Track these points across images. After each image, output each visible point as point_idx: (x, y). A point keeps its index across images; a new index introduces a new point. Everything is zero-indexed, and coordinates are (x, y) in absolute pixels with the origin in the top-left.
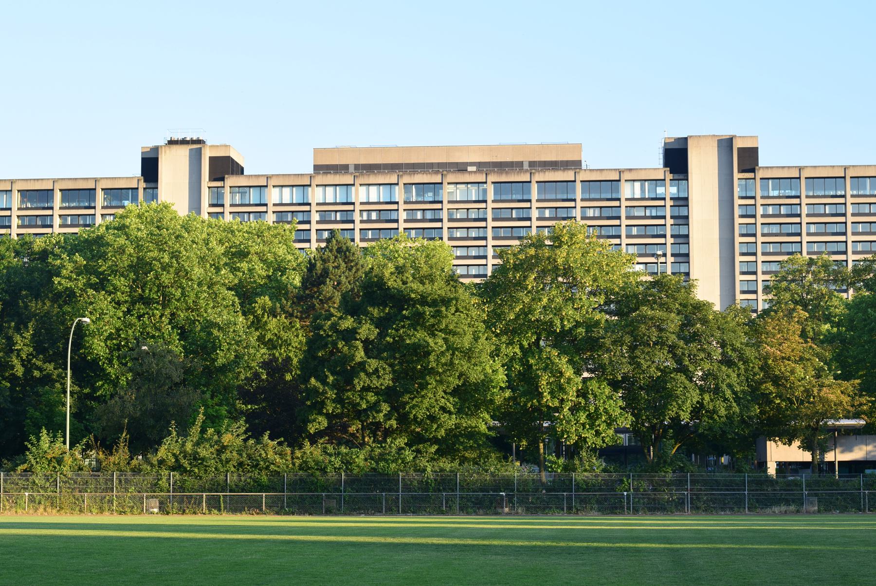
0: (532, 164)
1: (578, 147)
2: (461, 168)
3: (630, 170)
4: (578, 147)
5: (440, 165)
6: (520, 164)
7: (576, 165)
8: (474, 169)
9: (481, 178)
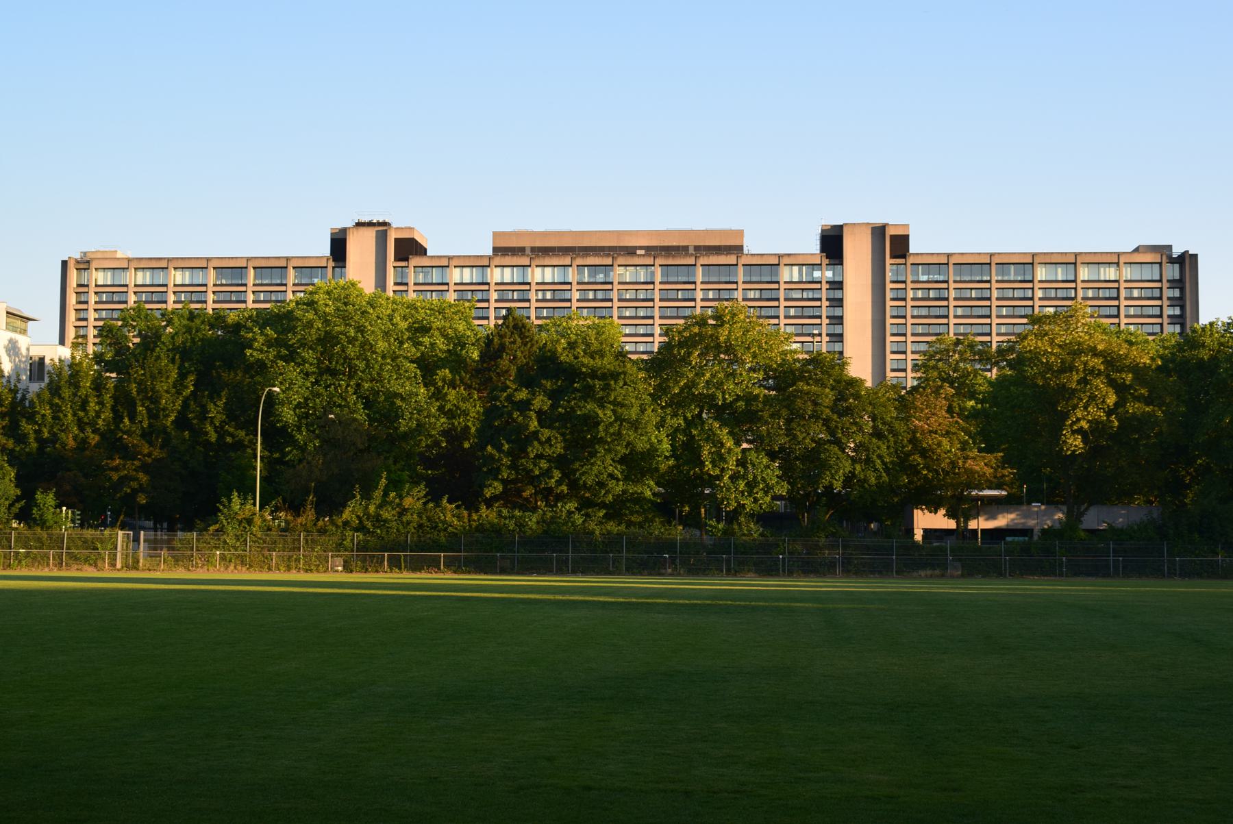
0: (697, 248)
1: (740, 233)
2: (630, 251)
3: (789, 255)
4: (740, 233)
5: (611, 249)
6: (686, 248)
7: (738, 249)
8: (643, 252)
9: (649, 261)
